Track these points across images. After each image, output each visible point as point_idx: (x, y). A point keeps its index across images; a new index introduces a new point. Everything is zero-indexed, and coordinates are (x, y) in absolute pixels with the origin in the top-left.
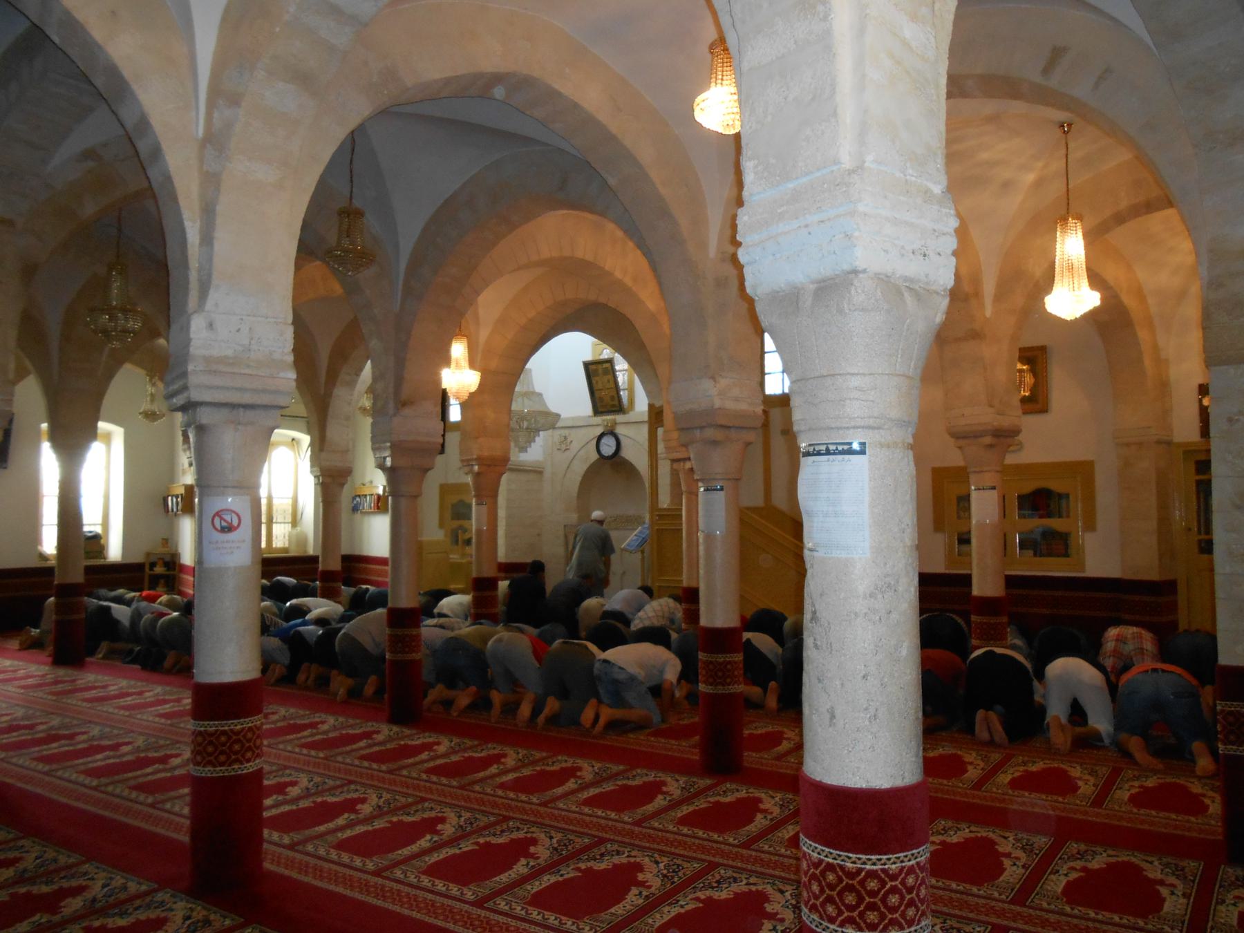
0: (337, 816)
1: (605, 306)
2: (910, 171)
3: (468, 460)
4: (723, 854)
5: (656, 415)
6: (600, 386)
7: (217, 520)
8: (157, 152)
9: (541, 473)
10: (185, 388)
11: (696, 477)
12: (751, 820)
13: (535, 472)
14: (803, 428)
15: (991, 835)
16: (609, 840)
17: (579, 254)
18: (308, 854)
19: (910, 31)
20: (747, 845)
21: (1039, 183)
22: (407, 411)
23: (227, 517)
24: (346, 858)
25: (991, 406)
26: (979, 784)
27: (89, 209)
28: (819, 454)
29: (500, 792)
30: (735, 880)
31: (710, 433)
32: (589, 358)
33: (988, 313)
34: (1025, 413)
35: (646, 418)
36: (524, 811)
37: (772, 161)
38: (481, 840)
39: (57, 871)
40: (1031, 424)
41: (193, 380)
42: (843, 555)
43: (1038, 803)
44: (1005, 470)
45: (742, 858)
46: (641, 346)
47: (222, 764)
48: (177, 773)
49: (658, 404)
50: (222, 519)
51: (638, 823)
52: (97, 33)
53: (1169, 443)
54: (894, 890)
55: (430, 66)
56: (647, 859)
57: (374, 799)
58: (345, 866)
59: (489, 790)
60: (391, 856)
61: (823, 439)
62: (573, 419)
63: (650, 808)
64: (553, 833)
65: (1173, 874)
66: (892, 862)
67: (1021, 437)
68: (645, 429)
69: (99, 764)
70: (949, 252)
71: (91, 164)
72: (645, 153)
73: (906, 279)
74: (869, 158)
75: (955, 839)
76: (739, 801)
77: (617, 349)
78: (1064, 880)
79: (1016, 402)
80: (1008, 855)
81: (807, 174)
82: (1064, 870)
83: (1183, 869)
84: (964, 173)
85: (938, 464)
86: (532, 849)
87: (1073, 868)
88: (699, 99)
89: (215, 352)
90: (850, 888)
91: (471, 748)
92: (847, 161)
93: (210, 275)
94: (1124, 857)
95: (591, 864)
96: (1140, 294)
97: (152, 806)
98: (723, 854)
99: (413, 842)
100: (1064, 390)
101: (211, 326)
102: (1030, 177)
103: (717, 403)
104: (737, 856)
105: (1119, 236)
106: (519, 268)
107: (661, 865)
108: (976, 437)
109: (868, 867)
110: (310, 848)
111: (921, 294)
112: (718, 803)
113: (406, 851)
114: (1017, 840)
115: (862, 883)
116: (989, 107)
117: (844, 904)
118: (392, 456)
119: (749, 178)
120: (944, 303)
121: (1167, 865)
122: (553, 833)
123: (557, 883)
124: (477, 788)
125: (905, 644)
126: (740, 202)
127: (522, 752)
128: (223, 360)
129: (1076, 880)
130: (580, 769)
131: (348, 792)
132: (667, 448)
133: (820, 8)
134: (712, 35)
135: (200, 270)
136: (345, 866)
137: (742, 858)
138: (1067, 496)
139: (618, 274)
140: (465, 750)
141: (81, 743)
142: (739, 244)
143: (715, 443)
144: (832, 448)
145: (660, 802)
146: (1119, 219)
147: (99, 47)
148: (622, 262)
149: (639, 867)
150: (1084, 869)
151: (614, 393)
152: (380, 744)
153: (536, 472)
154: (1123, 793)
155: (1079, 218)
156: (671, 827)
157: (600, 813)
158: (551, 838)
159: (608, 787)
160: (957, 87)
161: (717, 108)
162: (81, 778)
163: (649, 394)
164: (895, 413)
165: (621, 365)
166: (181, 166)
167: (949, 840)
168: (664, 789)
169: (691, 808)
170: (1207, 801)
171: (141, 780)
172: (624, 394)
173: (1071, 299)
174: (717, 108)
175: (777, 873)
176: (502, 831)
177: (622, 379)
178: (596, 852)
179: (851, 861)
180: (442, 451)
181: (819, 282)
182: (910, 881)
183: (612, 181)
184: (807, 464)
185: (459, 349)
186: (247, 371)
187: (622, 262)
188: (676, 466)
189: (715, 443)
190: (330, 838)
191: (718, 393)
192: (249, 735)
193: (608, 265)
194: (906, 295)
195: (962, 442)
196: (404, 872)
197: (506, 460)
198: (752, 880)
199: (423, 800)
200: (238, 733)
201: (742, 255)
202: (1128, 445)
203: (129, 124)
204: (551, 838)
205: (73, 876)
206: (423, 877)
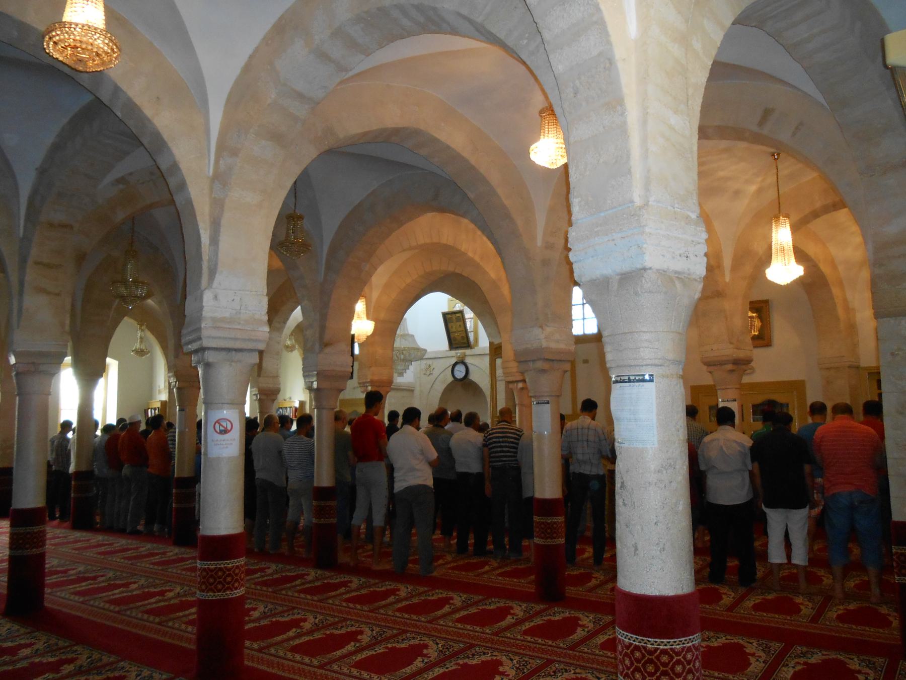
0: (289, 630)
1: (461, 275)
2: (677, 205)
3: (364, 383)
4: (556, 654)
5: (496, 351)
6: (454, 330)
7: (217, 426)
8: (183, 186)
9: (412, 391)
10: (200, 339)
11: (530, 394)
12: (573, 632)
13: (409, 390)
14: (613, 365)
15: (741, 641)
16: (477, 645)
17: (444, 241)
18: (271, 655)
19: (675, 120)
20: (573, 648)
21: (759, 191)
22: (328, 350)
23: (224, 424)
24: (298, 657)
25: (731, 343)
26: (731, 608)
27: (120, 216)
28: (624, 381)
29: (398, 614)
30: (566, 671)
31: (540, 365)
32: (446, 310)
33: (727, 280)
34: (755, 347)
35: (487, 351)
36: (415, 626)
37: (590, 199)
38: (390, 646)
39: (104, 666)
40: (760, 355)
41: (205, 333)
42: (640, 446)
43: (776, 619)
44: (742, 387)
45: (570, 656)
46: (485, 302)
47: (219, 591)
48: (172, 602)
49: (496, 342)
50: (220, 425)
51: (496, 634)
52: (148, 112)
53: (858, 367)
54: (679, 662)
55: (353, 125)
56: (504, 658)
57: (311, 619)
58: (298, 662)
59: (390, 613)
60: (329, 656)
61: (626, 372)
62: (436, 352)
63: (503, 624)
64: (438, 641)
65: (867, 666)
66: (677, 644)
67: (752, 364)
68: (487, 359)
69: (117, 596)
70: (702, 254)
71: (121, 186)
72: (494, 178)
73: (676, 272)
74: (652, 199)
75: (716, 644)
76: (565, 619)
77: (466, 304)
78: (791, 671)
79: (748, 340)
80: (753, 655)
81: (612, 208)
82: (792, 664)
83: (874, 664)
84: (709, 188)
85: (692, 384)
86: (425, 651)
87: (798, 663)
88: (532, 147)
89: (218, 315)
90: (650, 661)
91: (375, 584)
92: (638, 201)
93: (216, 265)
94: (833, 655)
95: (466, 661)
96: (833, 264)
97: (159, 624)
98: (556, 654)
99: (343, 647)
100: (782, 331)
101: (216, 297)
102: (753, 188)
103: (544, 344)
104: (565, 656)
105: (817, 225)
106: (404, 250)
107: (515, 662)
108: (721, 364)
109: (661, 647)
110: (273, 651)
111: (682, 278)
112: (549, 621)
113: (338, 653)
114: (759, 645)
115: (658, 658)
116: (724, 144)
117: (646, 672)
118: (317, 381)
119: (575, 209)
120: (700, 287)
121: (863, 661)
122: (438, 641)
123: (444, 673)
124: (382, 611)
125: (681, 503)
126: (570, 224)
127: (410, 588)
128: (223, 320)
129: (800, 671)
130: (452, 598)
131: (293, 614)
132: (506, 374)
133: (619, 108)
134: (538, 101)
135: (209, 260)
136: (298, 662)
137: (570, 656)
138: (787, 405)
139: (470, 254)
140: (370, 586)
141: (102, 582)
142: (570, 250)
143: (543, 371)
144: (632, 378)
145: (509, 620)
146: (815, 215)
147: (149, 120)
148: (473, 245)
149: (500, 663)
150: (805, 663)
151: (464, 335)
152: (310, 582)
153: (410, 390)
154: (832, 614)
155: (787, 216)
156: (519, 637)
157: (469, 627)
158: (437, 644)
159: (473, 610)
160: (703, 133)
161: (547, 151)
162: (107, 606)
163: (489, 335)
164: (671, 356)
165: (469, 314)
166: (199, 195)
167: (711, 644)
168: (512, 611)
169: (532, 624)
170: (891, 619)
171: (149, 607)
172: (471, 336)
173: (784, 271)
174: (547, 151)
175: (595, 666)
176: (403, 640)
177: (469, 325)
178: (469, 653)
179: (651, 643)
180: (352, 378)
181: (622, 274)
182: (689, 656)
183: (471, 196)
184: (616, 388)
185: (360, 307)
186: (239, 327)
187: (473, 245)
188: (511, 386)
189: (543, 371)
190: (286, 645)
191: (543, 337)
192: (237, 571)
193: (464, 248)
194: (677, 282)
195: (711, 368)
196: (340, 667)
197: (390, 382)
198: (577, 671)
199: (345, 620)
200: (229, 570)
201: (572, 257)
202: (828, 369)
203: (163, 167)
204: (437, 644)
205: (115, 670)
206: (353, 670)
